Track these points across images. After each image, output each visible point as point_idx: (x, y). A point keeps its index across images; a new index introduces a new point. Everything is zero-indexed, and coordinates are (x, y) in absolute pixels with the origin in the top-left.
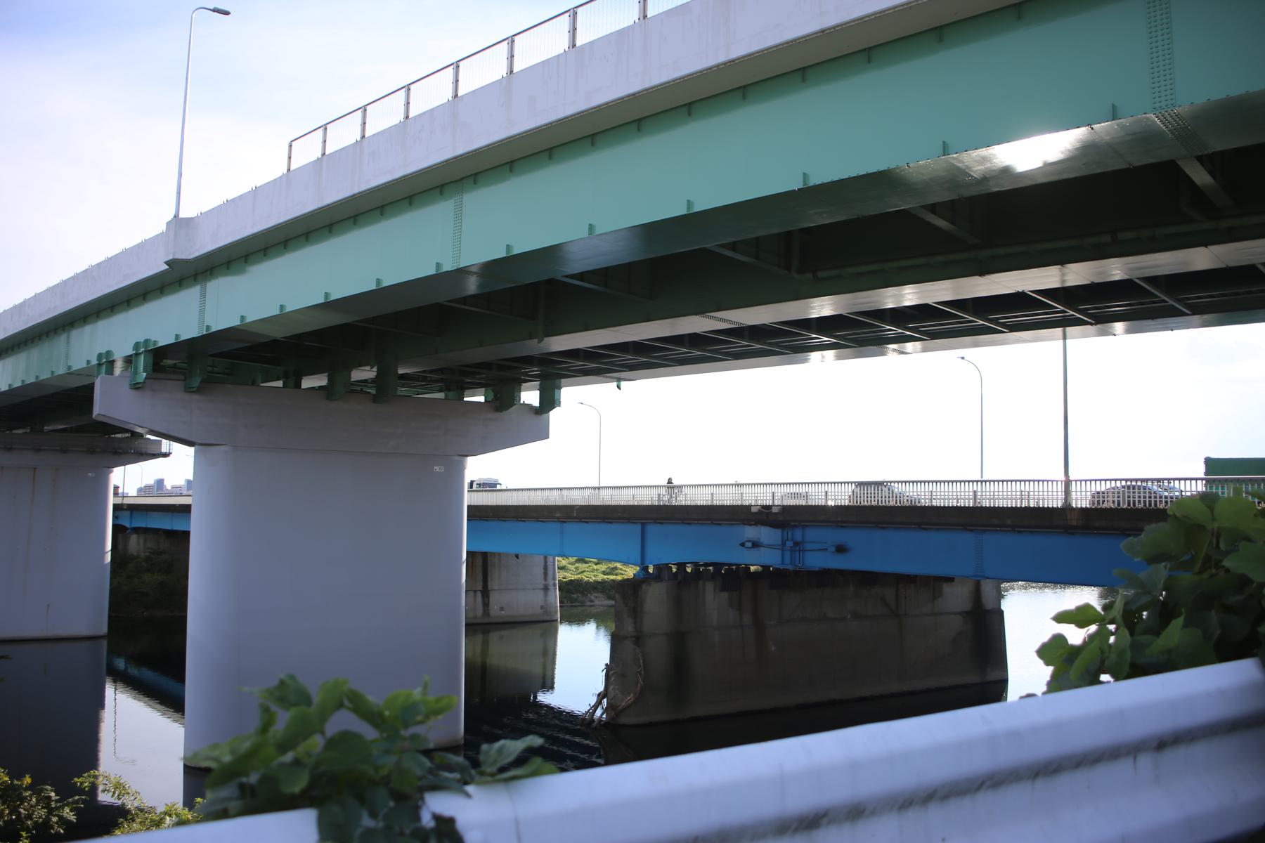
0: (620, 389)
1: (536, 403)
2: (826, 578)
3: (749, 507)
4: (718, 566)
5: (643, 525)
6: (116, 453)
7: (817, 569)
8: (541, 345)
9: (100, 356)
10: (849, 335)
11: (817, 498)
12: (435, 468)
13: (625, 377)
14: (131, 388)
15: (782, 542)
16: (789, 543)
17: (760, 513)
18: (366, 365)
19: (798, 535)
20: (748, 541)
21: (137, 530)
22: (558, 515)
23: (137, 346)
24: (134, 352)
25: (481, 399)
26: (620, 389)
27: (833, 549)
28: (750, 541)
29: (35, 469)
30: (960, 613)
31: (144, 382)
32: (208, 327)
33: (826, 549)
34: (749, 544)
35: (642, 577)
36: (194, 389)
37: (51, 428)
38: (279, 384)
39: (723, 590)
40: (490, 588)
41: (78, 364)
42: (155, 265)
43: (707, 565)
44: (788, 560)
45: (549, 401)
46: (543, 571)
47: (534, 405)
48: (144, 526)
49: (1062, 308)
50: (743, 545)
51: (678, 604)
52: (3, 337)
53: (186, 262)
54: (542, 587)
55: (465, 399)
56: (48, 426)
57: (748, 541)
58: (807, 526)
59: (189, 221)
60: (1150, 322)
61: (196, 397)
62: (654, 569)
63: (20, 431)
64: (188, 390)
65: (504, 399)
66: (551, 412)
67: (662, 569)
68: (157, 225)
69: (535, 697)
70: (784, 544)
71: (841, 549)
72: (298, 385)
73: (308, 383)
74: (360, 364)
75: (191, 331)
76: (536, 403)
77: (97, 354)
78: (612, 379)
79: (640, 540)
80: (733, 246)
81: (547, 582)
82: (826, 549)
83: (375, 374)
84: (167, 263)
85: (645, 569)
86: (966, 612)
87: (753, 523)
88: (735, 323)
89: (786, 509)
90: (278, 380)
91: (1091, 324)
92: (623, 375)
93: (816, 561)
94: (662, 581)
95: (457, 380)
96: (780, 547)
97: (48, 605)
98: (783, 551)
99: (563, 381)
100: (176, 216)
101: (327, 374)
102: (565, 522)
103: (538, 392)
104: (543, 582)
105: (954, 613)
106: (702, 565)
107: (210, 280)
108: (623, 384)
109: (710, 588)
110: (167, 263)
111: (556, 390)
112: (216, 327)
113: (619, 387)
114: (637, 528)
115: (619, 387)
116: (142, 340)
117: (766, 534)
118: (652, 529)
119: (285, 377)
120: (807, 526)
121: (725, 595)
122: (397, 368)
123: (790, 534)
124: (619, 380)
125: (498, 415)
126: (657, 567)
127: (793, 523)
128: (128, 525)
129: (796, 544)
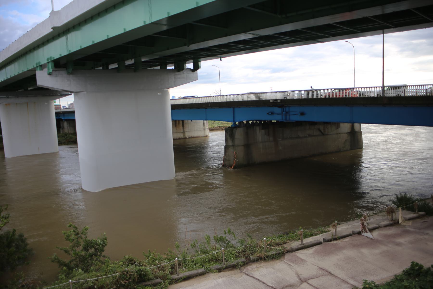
0: (221, 61)
1: (192, 68)
2: (298, 124)
3: (269, 100)
4: (260, 121)
5: (233, 108)
6: (53, 95)
7: (294, 121)
8: (189, 47)
9: (37, 64)
10: (302, 37)
11: (293, 96)
12: (158, 93)
13: (223, 56)
14: (48, 75)
15: (282, 111)
16: (284, 113)
17: (273, 102)
18: (130, 59)
19: (287, 109)
20: (269, 112)
21: (66, 120)
22: (204, 106)
23: (48, 59)
24: (47, 62)
25: (173, 67)
26: (221, 61)
27: (300, 114)
28: (270, 115)
29: (27, 103)
30: (347, 133)
31: (52, 72)
32: (70, 51)
33: (297, 114)
34: (270, 113)
35: (234, 126)
36: (70, 73)
37: (31, 88)
38: (101, 68)
39: (263, 129)
40: (185, 131)
41: (31, 67)
42: (48, 30)
43: (256, 121)
44: (284, 118)
45: (196, 67)
46: (203, 124)
47: (192, 68)
48: (68, 118)
49: (382, 22)
50: (268, 114)
51: (247, 135)
52: (1, 62)
53: (58, 27)
54: (203, 129)
55: (168, 68)
56: (29, 88)
57: (269, 112)
58: (290, 106)
59: (57, 12)
60: (417, 26)
61: (71, 76)
62: (238, 123)
63: (20, 91)
64: (69, 73)
65: (180, 68)
66: (198, 70)
67: (241, 124)
68: (46, 15)
69: (79, 268)
70: (282, 113)
71: (302, 114)
72: (108, 68)
73: (111, 67)
74: (127, 59)
75: (65, 53)
76: (192, 68)
77: (36, 63)
78: (218, 58)
79: (232, 113)
80: (254, 6)
81: (205, 128)
82: (297, 114)
83: (134, 62)
84: (52, 28)
85: (235, 123)
86: (349, 132)
87: (271, 106)
88: (258, 35)
89: (282, 100)
90: (100, 66)
91: (394, 28)
92: (222, 56)
93: (294, 118)
94: (241, 127)
95: (163, 63)
96: (281, 114)
97: (39, 148)
98: (282, 115)
99: (201, 59)
100: (53, 10)
101: (117, 63)
102: (207, 108)
103: (193, 64)
104: (203, 128)
105: (344, 133)
106: (255, 121)
107: (68, 34)
108: (222, 59)
109: (258, 128)
110: (52, 28)
111: (199, 63)
112: (72, 51)
113: (221, 60)
114: (231, 110)
115: (221, 60)
116: (49, 57)
117: (277, 110)
118: (237, 110)
119: (103, 66)
120: (290, 106)
121: (263, 131)
122: (141, 59)
123: (284, 109)
124: (221, 58)
125: (179, 73)
126: (239, 123)
127: (285, 106)
128: (63, 119)
129: (287, 113)
